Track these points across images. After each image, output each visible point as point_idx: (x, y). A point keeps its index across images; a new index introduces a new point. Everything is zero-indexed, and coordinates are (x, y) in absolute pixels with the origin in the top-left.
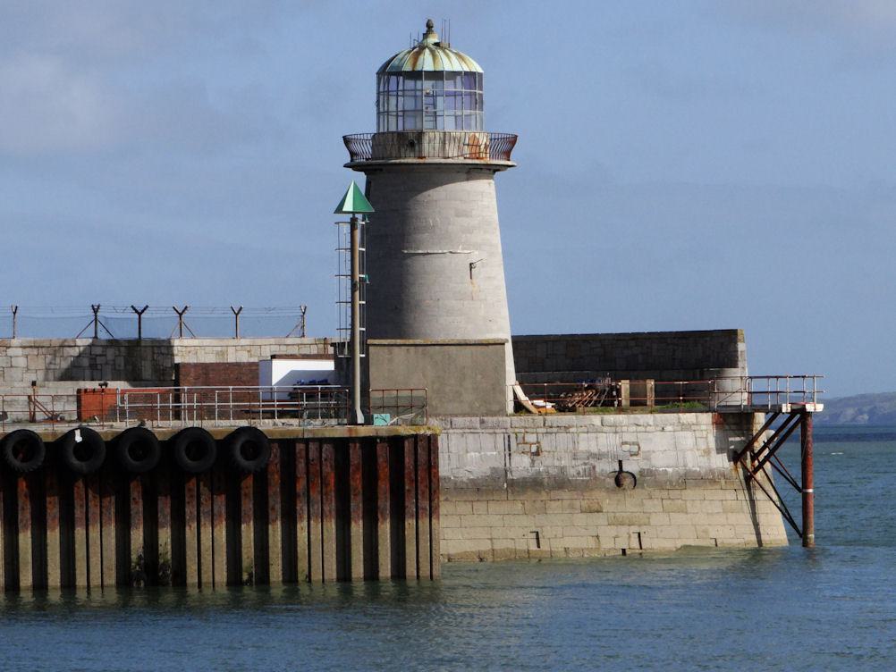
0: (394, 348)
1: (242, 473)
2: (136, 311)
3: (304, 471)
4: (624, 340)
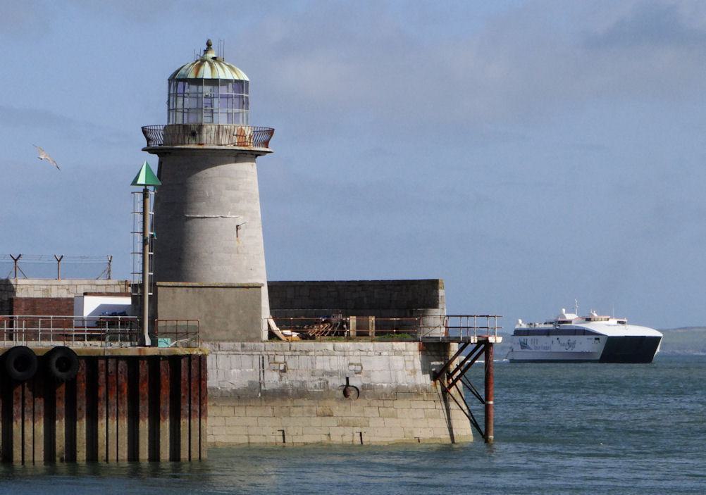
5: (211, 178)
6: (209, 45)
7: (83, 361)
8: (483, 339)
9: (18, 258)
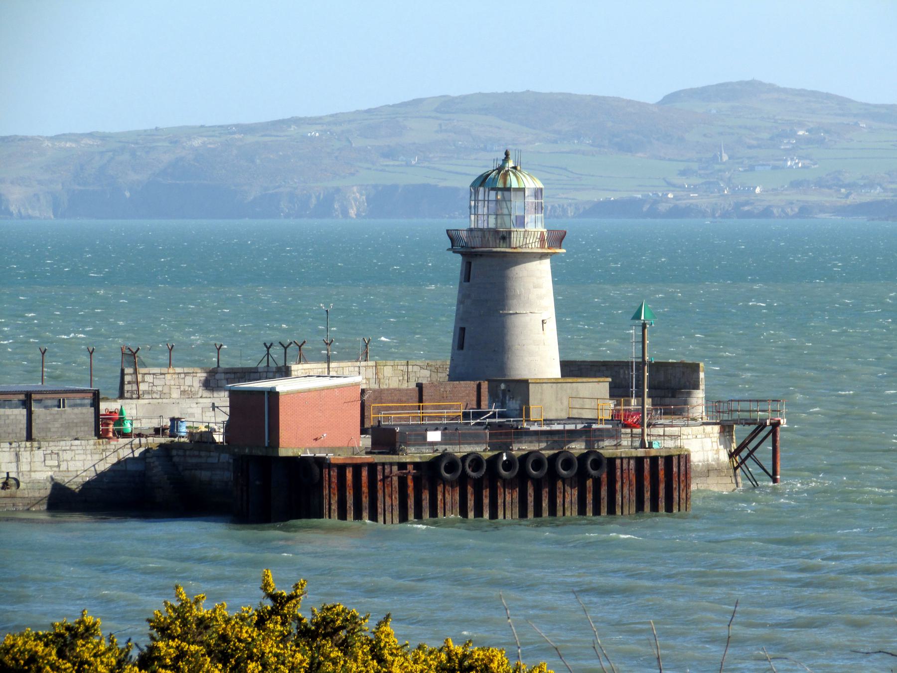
0: (544, 384)
1: (589, 476)
2: (283, 346)
3: (620, 477)
4: (597, 366)
5: (521, 277)
6: (507, 154)
7: (648, 460)
8: (776, 422)
9: (302, 344)
